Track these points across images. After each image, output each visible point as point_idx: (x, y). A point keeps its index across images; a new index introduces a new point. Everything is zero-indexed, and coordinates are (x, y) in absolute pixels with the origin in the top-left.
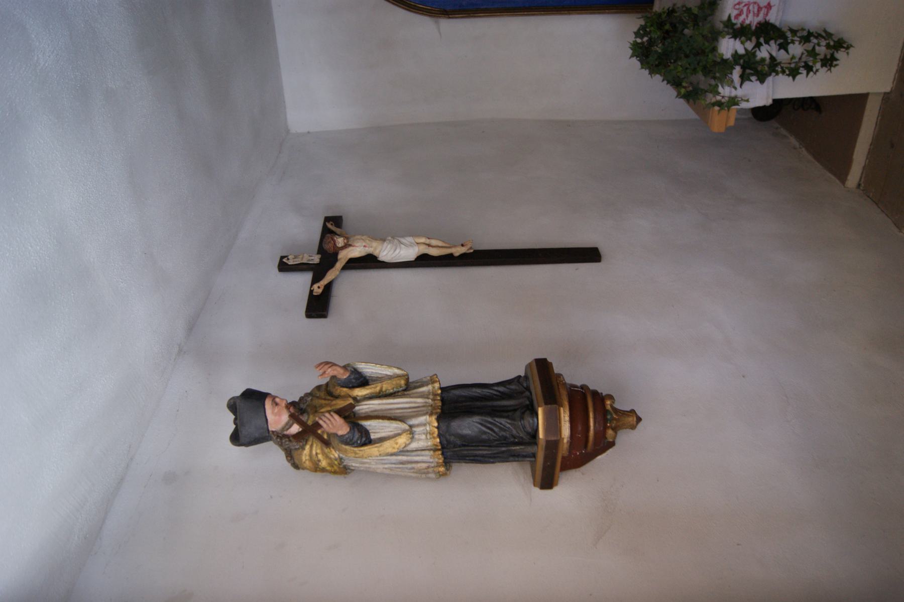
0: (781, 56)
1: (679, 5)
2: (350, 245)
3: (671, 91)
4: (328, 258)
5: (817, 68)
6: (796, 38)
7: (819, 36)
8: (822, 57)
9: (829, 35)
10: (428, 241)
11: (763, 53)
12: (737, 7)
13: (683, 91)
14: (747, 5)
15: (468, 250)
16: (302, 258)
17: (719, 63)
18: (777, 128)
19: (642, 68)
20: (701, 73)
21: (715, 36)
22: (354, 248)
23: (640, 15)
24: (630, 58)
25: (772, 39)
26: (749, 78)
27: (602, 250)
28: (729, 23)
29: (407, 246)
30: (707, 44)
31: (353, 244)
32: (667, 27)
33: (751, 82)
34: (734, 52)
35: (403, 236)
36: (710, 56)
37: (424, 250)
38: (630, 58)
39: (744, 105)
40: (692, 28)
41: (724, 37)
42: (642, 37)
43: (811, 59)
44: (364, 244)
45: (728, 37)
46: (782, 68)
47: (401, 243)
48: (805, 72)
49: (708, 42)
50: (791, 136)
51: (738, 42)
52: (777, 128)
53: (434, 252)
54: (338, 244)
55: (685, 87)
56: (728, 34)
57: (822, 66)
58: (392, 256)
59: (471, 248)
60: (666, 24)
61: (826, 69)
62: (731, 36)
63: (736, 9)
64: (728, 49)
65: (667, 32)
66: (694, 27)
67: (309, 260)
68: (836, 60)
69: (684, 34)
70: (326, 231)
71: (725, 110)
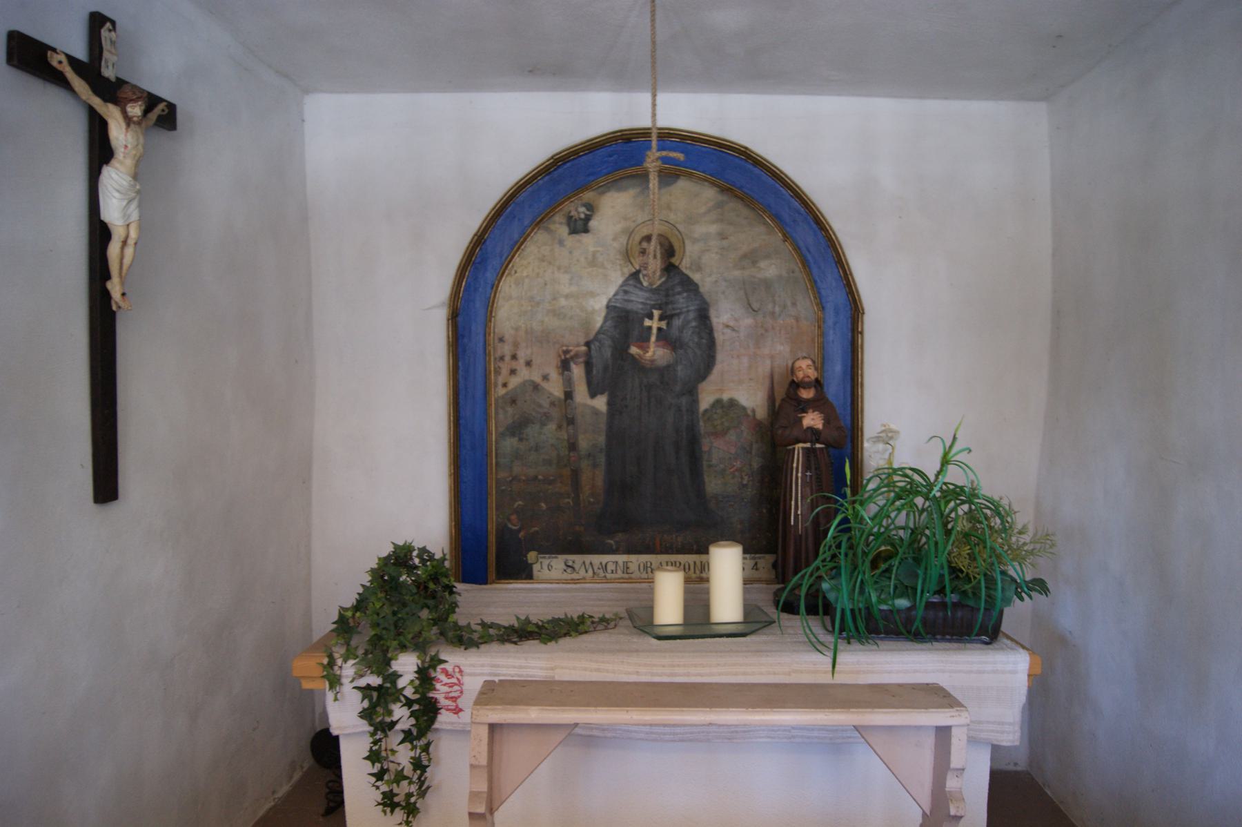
0: (394, 738)
1: (458, 598)
2: (128, 125)
3: (349, 600)
4: (112, 91)
5: (381, 787)
6: (418, 751)
7: (421, 782)
8: (396, 790)
9: (422, 793)
10: (131, 242)
11: (400, 713)
12: (457, 670)
13: (349, 614)
14: (460, 683)
15: (116, 303)
16: (110, 52)
17: (385, 655)
18: (302, 767)
19: (379, 559)
20: (373, 633)
21: (419, 646)
22: (124, 129)
23: (447, 551)
24: (393, 543)
25: (417, 719)
26: (366, 698)
27: (113, 508)
28: (436, 661)
29: (124, 209)
30: (410, 636)
31: (129, 130)
32: (432, 586)
33: (360, 701)
34: (399, 673)
35: (140, 206)
36: (395, 643)
37: (117, 234)
38: (393, 543)
39: (330, 695)
40: (430, 617)
41: (418, 658)
42: (419, 556)
43: (393, 777)
44: (129, 146)
45: (419, 662)
46: (380, 740)
47: (130, 201)
48: (375, 771)
49: (413, 638)
50: (291, 786)
51: (412, 676)
52: (302, 767)
53: (113, 250)
54: (131, 107)
55: (354, 615)
56: (423, 662)
57: (383, 793)
58: (109, 186)
59: (119, 307)
60: (435, 584)
61: (380, 800)
62: (420, 666)
63: (454, 669)
64: (405, 665)
65: (426, 588)
66: (432, 619)
67: (107, 62)
68: (392, 812)
69: (422, 608)
70: (152, 101)
71: (323, 672)
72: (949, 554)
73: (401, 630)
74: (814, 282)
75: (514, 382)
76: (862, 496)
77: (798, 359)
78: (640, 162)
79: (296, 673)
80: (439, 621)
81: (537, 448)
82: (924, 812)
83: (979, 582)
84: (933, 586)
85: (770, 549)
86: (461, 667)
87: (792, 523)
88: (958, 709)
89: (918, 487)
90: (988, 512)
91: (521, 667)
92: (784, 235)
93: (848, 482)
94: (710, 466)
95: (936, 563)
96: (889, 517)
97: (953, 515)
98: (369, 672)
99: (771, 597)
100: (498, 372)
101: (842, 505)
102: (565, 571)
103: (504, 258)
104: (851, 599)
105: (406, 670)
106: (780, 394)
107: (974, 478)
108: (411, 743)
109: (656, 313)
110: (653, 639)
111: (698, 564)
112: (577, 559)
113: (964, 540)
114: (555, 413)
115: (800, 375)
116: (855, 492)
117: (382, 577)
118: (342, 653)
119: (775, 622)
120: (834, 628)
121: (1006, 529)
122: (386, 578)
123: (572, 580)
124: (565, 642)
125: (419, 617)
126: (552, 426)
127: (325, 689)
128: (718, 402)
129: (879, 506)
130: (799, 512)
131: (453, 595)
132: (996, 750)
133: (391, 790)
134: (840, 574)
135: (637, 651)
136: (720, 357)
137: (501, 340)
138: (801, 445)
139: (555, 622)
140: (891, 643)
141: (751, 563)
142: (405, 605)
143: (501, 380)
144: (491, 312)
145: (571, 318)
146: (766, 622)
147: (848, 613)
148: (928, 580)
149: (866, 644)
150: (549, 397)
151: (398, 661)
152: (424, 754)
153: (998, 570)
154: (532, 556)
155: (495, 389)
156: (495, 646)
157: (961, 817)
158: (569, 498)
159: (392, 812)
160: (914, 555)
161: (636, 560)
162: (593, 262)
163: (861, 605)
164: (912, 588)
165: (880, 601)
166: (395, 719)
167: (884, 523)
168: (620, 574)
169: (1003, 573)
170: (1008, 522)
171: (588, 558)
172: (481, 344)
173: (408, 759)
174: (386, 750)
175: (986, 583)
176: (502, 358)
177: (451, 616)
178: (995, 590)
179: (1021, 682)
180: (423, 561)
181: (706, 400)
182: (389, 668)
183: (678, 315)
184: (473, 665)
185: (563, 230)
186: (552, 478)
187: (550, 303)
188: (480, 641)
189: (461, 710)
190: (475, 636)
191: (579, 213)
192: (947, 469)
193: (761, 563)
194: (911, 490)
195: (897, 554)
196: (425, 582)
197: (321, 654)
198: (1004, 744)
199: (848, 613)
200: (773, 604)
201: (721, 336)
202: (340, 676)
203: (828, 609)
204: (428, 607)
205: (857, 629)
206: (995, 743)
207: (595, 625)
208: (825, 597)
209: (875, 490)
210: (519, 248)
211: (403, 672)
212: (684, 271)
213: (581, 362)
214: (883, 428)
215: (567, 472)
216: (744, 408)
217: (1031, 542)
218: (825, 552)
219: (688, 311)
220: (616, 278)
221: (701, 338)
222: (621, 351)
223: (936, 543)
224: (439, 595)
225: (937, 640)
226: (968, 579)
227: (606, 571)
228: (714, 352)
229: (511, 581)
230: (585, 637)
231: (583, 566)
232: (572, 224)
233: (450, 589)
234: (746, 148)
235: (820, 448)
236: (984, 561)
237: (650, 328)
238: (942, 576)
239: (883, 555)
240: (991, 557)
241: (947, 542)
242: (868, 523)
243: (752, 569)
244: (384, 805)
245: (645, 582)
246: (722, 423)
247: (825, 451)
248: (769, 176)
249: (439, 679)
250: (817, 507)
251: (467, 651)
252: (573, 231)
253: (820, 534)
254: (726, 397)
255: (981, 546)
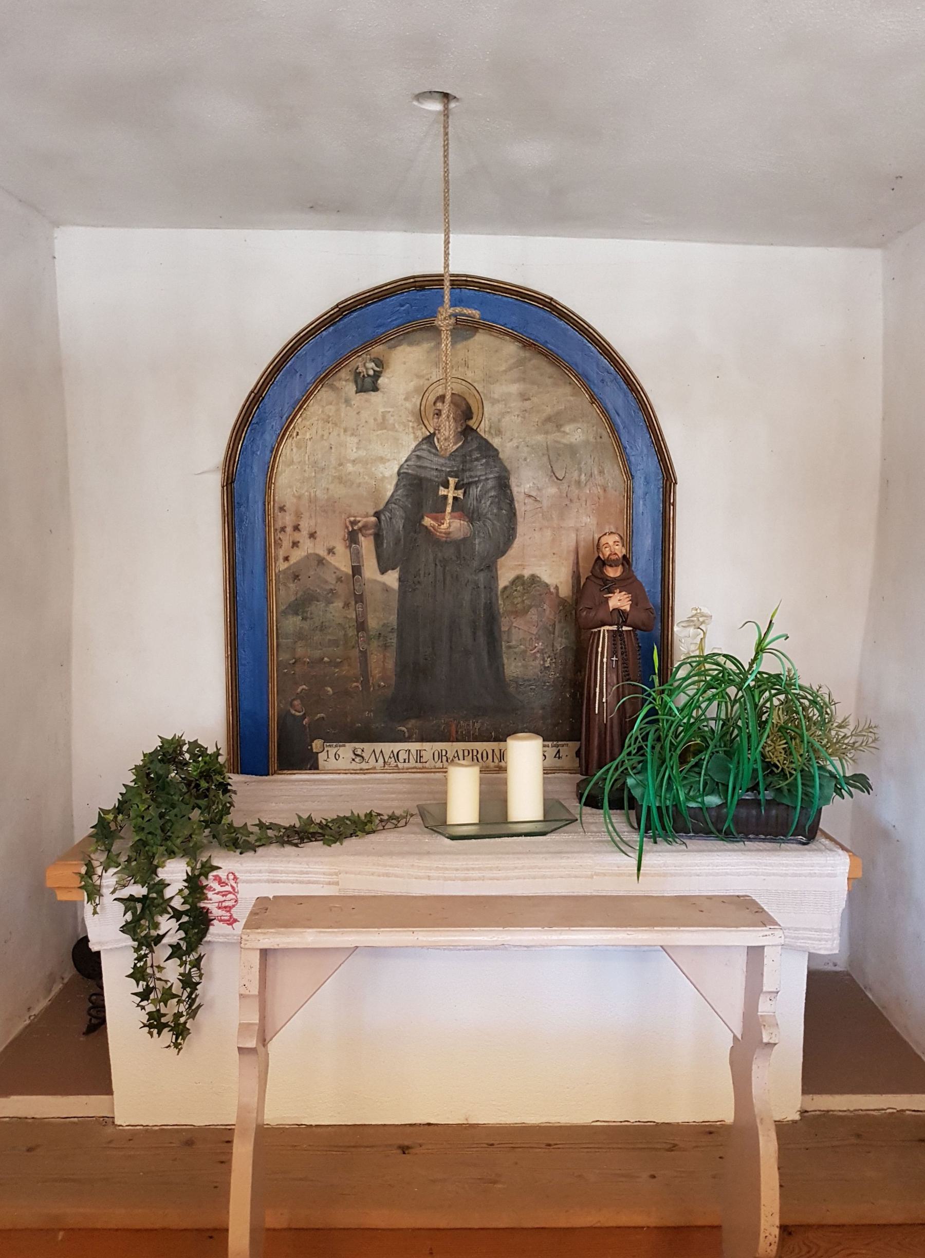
0: (162, 952)
3: (110, 802)
7: (191, 1000)
9: (193, 1013)
11: (167, 925)
12: (231, 877)
13: (110, 817)
14: (234, 891)
19: (145, 755)
20: (137, 838)
21: (190, 851)
30: (179, 841)
32: (204, 784)
34: (167, 882)
39: (89, 908)
40: (202, 819)
41: (188, 864)
43: (160, 996)
45: (189, 869)
46: (146, 956)
48: (140, 989)
51: (181, 885)
55: (116, 817)
56: (193, 869)
60: (208, 783)
65: (197, 786)
68: (159, 1033)
69: (193, 809)
72: (764, 748)
73: (169, 834)
74: (622, 449)
75: (297, 556)
76: (671, 685)
77: (605, 534)
78: (434, 314)
79: (50, 884)
80: (211, 823)
81: (322, 628)
82: (735, 1036)
83: (796, 779)
84: (747, 783)
85: (573, 736)
86: (236, 874)
87: (597, 712)
88: (772, 927)
89: (730, 675)
90: (807, 703)
91: (302, 873)
92: (591, 396)
93: (657, 671)
94: (509, 647)
95: (749, 756)
96: (700, 707)
97: (768, 705)
98: (133, 881)
99: (574, 788)
100: (278, 544)
101: (649, 695)
102: (353, 760)
103: (284, 417)
104: (658, 795)
105: (174, 878)
106: (585, 574)
107: (791, 667)
108: (181, 959)
109: (452, 481)
110: (446, 839)
111: (497, 753)
112: (368, 747)
113: (780, 733)
114: (341, 589)
115: (607, 552)
116: (663, 681)
117: (148, 774)
118: (102, 860)
119: (577, 820)
120: (639, 824)
121: (823, 724)
122: (152, 776)
123: (361, 769)
124: (351, 843)
125: (190, 819)
126: (339, 604)
127: (84, 900)
128: (519, 578)
129: (689, 696)
130: (604, 700)
131: (228, 794)
132: (812, 957)
133: (158, 1011)
134: (646, 769)
135: (428, 853)
136: (521, 529)
137: (282, 509)
138: (607, 628)
139: (340, 820)
140: (700, 842)
141: (552, 751)
142: (173, 806)
143: (282, 553)
144: (271, 478)
145: (359, 485)
146: (567, 820)
147: (654, 811)
148: (740, 776)
149: (674, 843)
150: (335, 573)
151: (165, 869)
152: (195, 969)
153: (816, 765)
154: (317, 744)
155: (275, 564)
156: (274, 849)
157: (775, 1044)
158: (357, 682)
159: (159, 1033)
160: (725, 749)
161: (429, 748)
162: (383, 424)
163: (668, 803)
164: (723, 784)
165: (687, 800)
166: (161, 932)
167: (694, 714)
168: (412, 763)
169: (821, 768)
170: (827, 713)
171: (379, 746)
172: (260, 512)
173: (177, 976)
174: (152, 966)
175: (802, 779)
176: (283, 529)
177: (224, 817)
178: (813, 787)
179: (841, 887)
180: (194, 757)
181: (505, 578)
182: (154, 876)
183: (476, 483)
184: (247, 872)
185: (351, 388)
186: (338, 660)
187: (335, 468)
188: (257, 844)
189: (236, 921)
190: (252, 839)
191: (367, 369)
192: (762, 658)
193: (564, 751)
194: (723, 679)
195: (707, 747)
196: (196, 780)
197: (76, 862)
198: (822, 952)
199: (654, 811)
200: (575, 797)
201: (521, 506)
202: (100, 886)
203: (633, 804)
204: (200, 808)
205: (664, 828)
206: (812, 951)
207: (383, 824)
208: (629, 790)
209: (685, 679)
210: (301, 407)
211: (170, 880)
212: (482, 434)
213: (371, 534)
214: (694, 612)
215: (355, 653)
216: (547, 585)
217: (852, 735)
218: (629, 746)
219: (487, 479)
220: (408, 443)
221: (500, 509)
222: (414, 522)
223: (749, 737)
224: (211, 794)
225: (750, 840)
226: (783, 775)
227: (398, 760)
228: (516, 524)
229: (295, 772)
230: (372, 837)
231: (373, 754)
232: (359, 381)
233: (224, 788)
234: (551, 299)
235: (626, 631)
236: (801, 755)
237: (445, 497)
238: (755, 771)
239: (692, 749)
240: (808, 752)
241: (762, 735)
242: (676, 715)
243: (555, 757)
244: (150, 1026)
245: (439, 772)
246: (523, 601)
247: (632, 632)
248: (577, 331)
249: (211, 887)
250: (623, 698)
251: (243, 855)
252: (361, 390)
253: (626, 725)
254: (527, 573)
255: (798, 741)
